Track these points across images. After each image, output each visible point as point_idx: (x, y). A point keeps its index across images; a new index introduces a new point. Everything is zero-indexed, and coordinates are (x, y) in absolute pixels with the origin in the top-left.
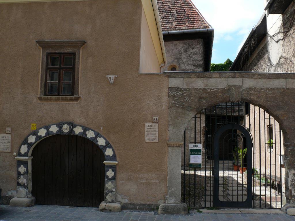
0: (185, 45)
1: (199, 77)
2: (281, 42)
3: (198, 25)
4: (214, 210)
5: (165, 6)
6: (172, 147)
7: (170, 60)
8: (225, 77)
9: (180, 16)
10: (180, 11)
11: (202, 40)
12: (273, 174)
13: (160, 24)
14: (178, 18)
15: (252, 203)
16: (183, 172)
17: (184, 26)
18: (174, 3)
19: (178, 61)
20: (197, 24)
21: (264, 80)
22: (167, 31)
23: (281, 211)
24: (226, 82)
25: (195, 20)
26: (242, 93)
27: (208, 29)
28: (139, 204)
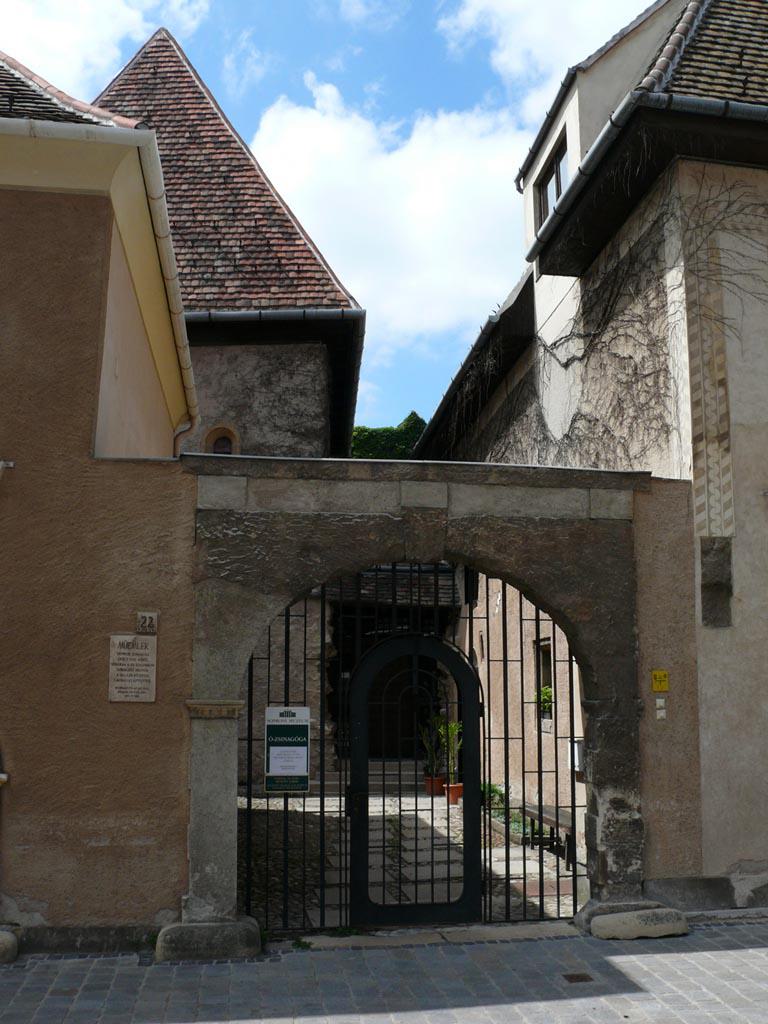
0: (266, 362)
1: (302, 477)
2: (577, 366)
3: (312, 295)
4: (353, 937)
5: (201, 222)
6: (206, 719)
7: (213, 413)
8: (390, 479)
9: (250, 262)
10: (254, 242)
11: (325, 345)
12: (548, 800)
13: (175, 284)
14: (243, 265)
15: (351, 896)
16: (242, 802)
17: (264, 295)
18: (234, 214)
19: (239, 415)
20: (309, 292)
21: (519, 492)
22: (204, 309)
23: (572, 928)
24: (394, 493)
25: (303, 278)
26: (447, 532)
27: (345, 309)
28: (84, 930)
